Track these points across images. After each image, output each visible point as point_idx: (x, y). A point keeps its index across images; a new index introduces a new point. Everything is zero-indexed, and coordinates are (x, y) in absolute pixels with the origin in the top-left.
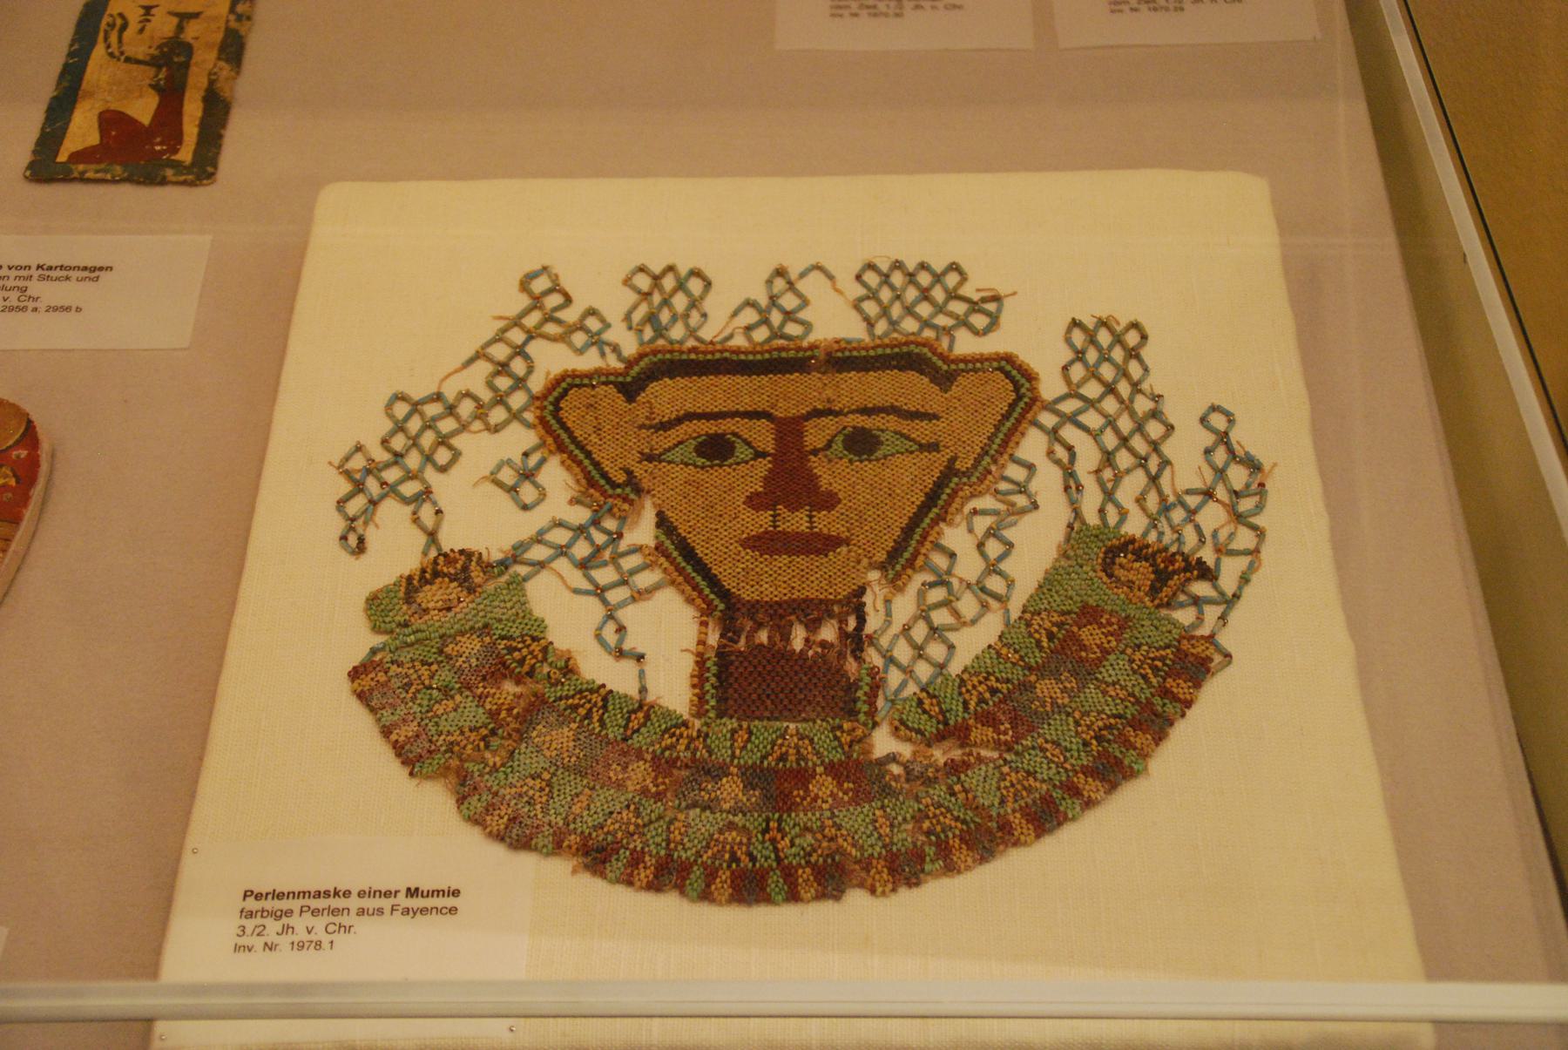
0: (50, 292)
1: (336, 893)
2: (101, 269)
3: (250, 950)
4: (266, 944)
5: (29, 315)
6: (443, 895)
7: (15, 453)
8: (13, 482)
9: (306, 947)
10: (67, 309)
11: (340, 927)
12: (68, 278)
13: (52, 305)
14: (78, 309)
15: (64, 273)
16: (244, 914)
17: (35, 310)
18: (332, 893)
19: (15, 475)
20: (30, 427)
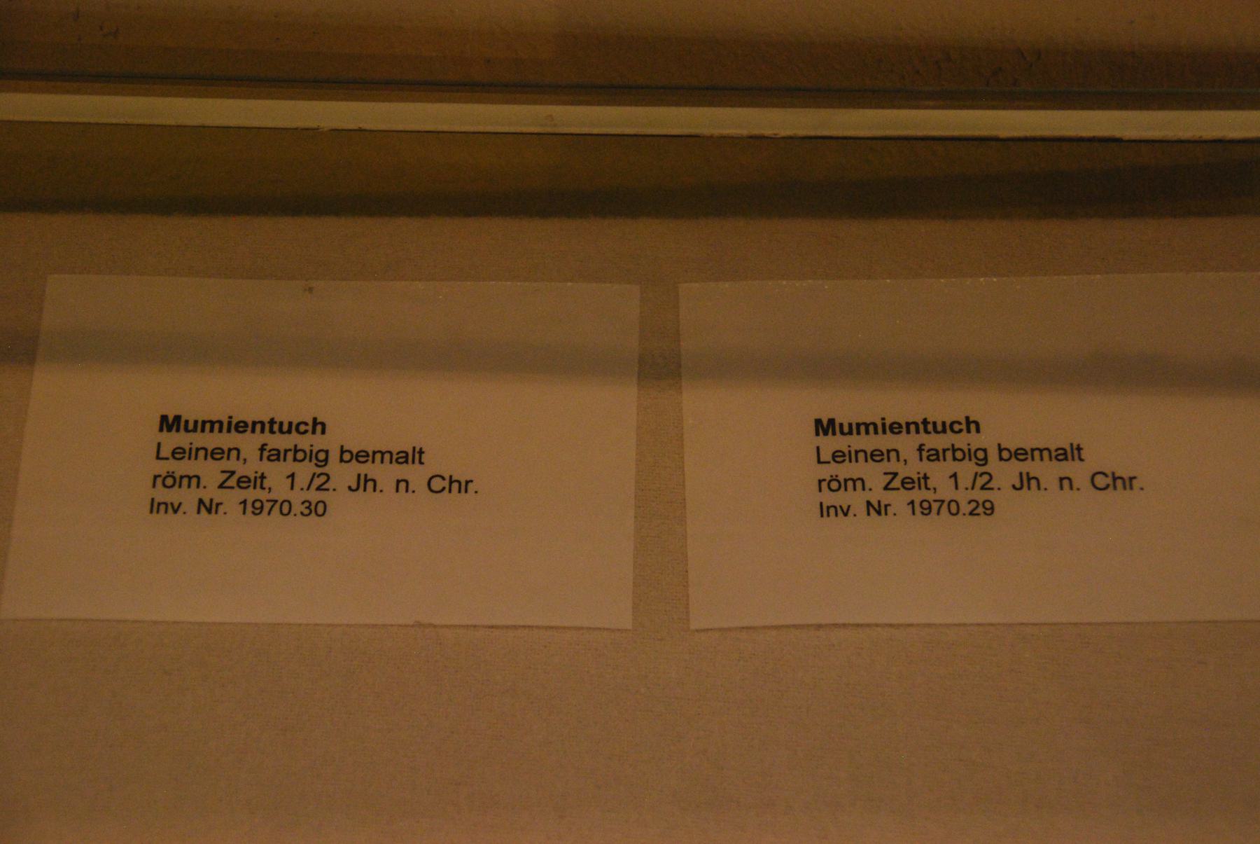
3: (846, 514)
4: (201, 501)
6: (876, 432)
9: (266, 510)
11: (451, 482)
16: (266, 454)
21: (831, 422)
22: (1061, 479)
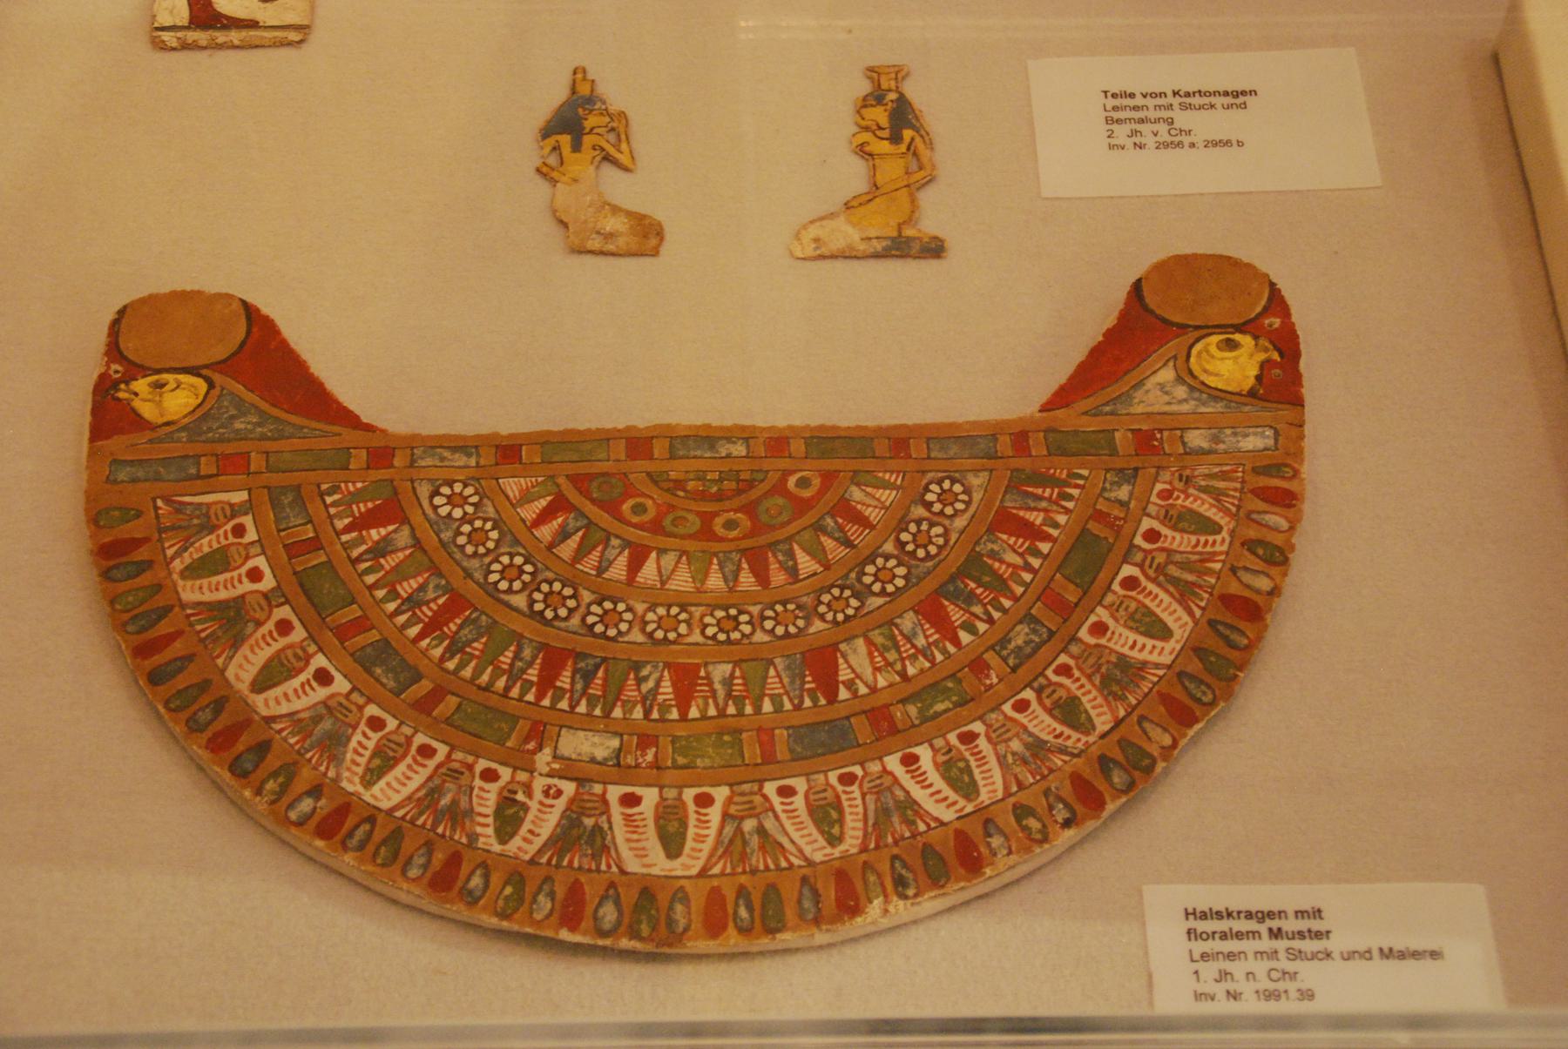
0: (1203, 124)
1: (1229, 915)
2: (1244, 93)
5: (1185, 152)
7: (1267, 322)
8: (1276, 356)
10: (1228, 143)
12: (1212, 106)
13: (1210, 139)
14: (1240, 144)
15: (1206, 100)
17: (1192, 145)
18: (1225, 914)
19: (1277, 349)
20: (1275, 292)
21: (1391, 950)
22: (1248, 974)
